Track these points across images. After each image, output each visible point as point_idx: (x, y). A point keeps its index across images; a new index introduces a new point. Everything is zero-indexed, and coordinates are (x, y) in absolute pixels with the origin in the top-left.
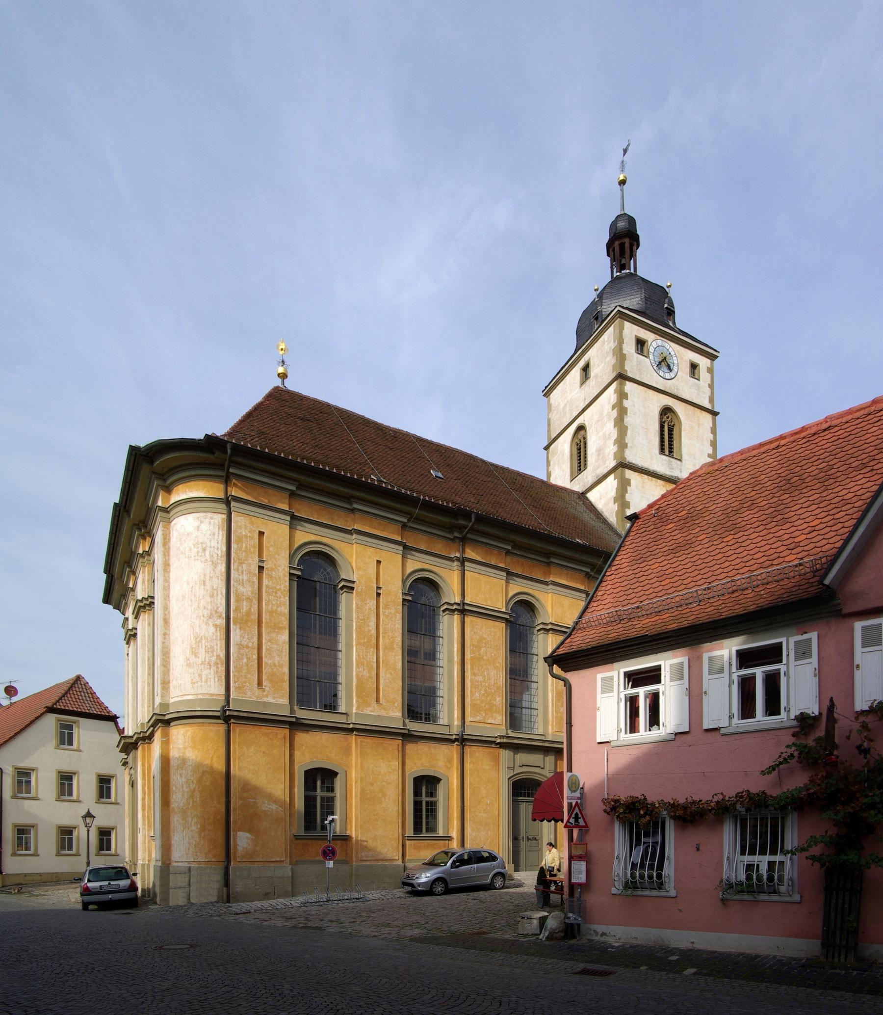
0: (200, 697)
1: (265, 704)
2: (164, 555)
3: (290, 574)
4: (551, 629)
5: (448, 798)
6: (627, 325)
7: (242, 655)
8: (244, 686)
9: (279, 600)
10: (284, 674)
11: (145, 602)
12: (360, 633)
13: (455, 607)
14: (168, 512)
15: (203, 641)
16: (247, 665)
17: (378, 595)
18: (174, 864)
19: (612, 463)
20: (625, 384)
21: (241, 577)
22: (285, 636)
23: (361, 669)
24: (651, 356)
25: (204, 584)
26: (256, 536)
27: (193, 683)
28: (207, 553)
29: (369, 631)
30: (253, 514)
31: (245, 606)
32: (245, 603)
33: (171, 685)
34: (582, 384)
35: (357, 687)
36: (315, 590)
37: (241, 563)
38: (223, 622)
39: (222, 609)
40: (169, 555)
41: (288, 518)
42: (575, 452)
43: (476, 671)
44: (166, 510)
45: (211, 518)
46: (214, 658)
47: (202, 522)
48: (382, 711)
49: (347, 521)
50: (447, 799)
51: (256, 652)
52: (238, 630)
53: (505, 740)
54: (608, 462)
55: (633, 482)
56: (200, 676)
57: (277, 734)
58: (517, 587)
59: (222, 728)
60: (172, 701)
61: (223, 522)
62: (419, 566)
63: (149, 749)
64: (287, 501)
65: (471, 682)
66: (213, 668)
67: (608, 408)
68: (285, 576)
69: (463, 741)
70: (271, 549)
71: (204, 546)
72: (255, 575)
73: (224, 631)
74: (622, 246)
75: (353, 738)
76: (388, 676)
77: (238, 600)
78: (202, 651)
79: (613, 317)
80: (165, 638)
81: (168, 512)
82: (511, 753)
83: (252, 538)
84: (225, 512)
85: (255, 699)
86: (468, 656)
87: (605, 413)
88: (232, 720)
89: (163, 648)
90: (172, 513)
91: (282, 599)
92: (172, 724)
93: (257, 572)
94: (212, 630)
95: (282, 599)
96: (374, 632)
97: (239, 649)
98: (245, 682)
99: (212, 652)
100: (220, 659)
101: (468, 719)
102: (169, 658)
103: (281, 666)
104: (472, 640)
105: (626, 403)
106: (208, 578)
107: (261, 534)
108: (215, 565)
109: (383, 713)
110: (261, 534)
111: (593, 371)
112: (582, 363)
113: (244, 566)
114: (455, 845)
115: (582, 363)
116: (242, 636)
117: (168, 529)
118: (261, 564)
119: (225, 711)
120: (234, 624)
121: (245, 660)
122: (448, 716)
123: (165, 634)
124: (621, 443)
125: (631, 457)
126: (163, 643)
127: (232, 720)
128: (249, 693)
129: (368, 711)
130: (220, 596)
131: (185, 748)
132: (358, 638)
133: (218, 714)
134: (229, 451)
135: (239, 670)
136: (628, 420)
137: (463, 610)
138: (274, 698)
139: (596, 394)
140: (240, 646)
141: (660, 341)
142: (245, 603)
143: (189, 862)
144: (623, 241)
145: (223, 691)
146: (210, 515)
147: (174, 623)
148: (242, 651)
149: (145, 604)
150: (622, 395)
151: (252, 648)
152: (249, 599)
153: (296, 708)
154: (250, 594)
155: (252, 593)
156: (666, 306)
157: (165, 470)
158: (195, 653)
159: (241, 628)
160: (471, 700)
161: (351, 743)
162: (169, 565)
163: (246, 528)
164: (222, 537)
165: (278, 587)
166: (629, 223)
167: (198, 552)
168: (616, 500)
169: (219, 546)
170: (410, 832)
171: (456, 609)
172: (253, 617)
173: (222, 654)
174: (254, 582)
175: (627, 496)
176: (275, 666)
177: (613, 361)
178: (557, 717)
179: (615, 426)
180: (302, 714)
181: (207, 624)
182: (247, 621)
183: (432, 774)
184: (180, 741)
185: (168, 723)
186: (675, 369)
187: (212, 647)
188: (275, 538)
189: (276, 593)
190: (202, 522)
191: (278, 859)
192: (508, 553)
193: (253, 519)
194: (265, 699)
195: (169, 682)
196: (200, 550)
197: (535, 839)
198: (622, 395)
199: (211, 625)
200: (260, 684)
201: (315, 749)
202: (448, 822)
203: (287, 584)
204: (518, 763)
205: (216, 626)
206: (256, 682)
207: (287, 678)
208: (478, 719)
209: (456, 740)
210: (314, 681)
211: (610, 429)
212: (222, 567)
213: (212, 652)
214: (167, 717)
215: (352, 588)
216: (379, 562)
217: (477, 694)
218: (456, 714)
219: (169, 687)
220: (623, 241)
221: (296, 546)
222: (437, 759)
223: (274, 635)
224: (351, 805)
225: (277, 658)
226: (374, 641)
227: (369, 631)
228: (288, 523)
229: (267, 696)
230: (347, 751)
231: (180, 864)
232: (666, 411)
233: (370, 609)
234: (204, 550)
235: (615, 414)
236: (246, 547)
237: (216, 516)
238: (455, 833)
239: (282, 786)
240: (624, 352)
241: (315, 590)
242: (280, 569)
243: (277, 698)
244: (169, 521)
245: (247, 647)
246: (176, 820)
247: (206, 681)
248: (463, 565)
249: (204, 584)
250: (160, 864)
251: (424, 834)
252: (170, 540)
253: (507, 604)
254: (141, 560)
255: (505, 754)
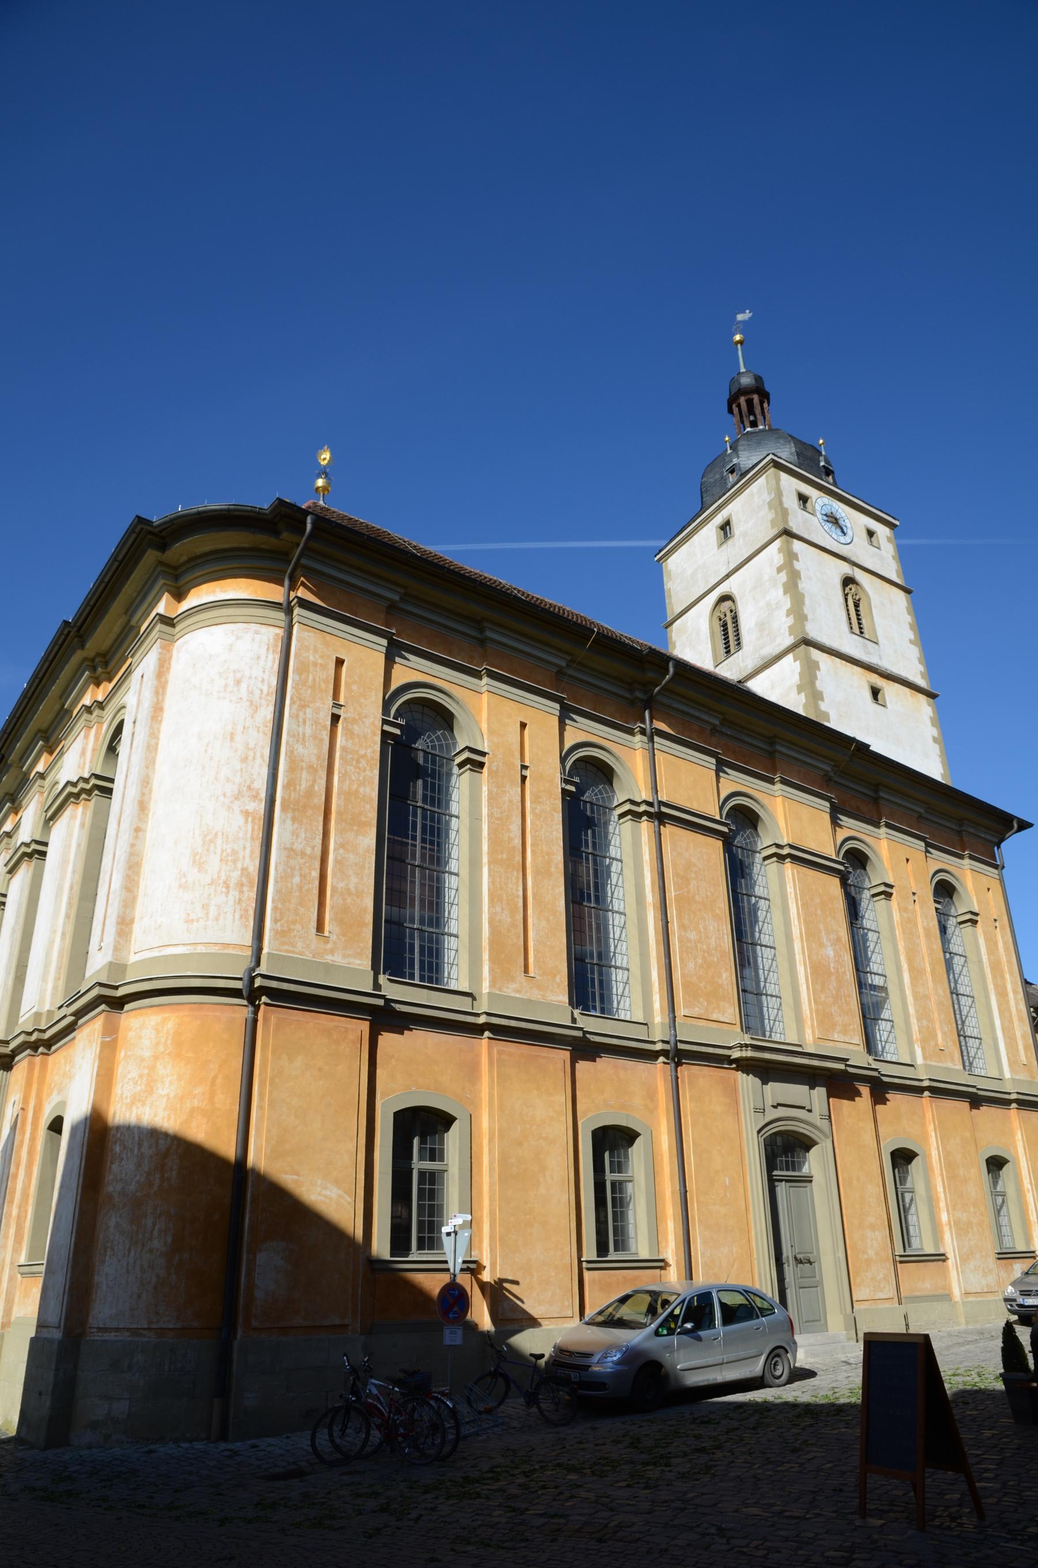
0: (201, 949)
1: (328, 968)
2: (157, 693)
3: (384, 732)
4: (789, 855)
5: (653, 1174)
6: (784, 476)
7: (293, 869)
8: (290, 930)
9: (361, 780)
10: (365, 910)
11: (81, 785)
12: (494, 842)
13: (643, 808)
14: (173, 626)
15: (219, 841)
16: (300, 889)
17: (524, 778)
18: (98, 1337)
19: (789, 641)
20: (792, 543)
21: (301, 730)
22: (369, 840)
23: (498, 909)
24: (818, 514)
25: (232, 739)
26: (332, 665)
27: (189, 921)
28: (244, 686)
29: (510, 839)
30: (329, 630)
31: (304, 780)
32: (304, 775)
33: (136, 927)
34: (720, 545)
35: (492, 942)
36: (415, 763)
37: (303, 707)
38: (261, 807)
39: (261, 785)
40: (164, 693)
41: (385, 642)
42: (719, 630)
43: (686, 922)
44: (168, 621)
45: (257, 632)
46: (236, 874)
47: (238, 638)
48: (535, 992)
49: (472, 657)
50: (647, 1171)
51: (317, 864)
52: (289, 822)
53: (749, 1053)
54: (778, 641)
55: (822, 665)
56: (205, 907)
57: (347, 1030)
58: (734, 782)
59: (247, 1012)
60: (133, 959)
61: (276, 640)
62: (582, 737)
63: (44, 1066)
64: (382, 616)
65: (680, 941)
66: (234, 894)
67: (769, 571)
68: (374, 734)
69: (679, 1056)
70: (355, 687)
71: (239, 675)
72: (324, 727)
73: (260, 824)
74: (750, 403)
75: (484, 1043)
76: (544, 923)
77: (292, 769)
78: (214, 862)
79: (764, 467)
80: (136, 838)
81: (173, 626)
82: (758, 1081)
83: (324, 667)
84: (282, 624)
85: (309, 956)
86: (671, 893)
87: (766, 577)
88: (264, 999)
89: (131, 854)
90: (178, 628)
91: (368, 773)
92: (127, 1007)
93: (329, 723)
94: (240, 820)
95: (368, 773)
96: (518, 842)
97: (288, 857)
98: (294, 922)
99: (235, 861)
100: (248, 875)
101: (681, 1011)
102: (138, 874)
103: (359, 894)
104: (674, 866)
105: (797, 565)
106: (240, 728)
107: (340, 662)
108: (255, 708)
109: (535, 995)
110: (340, 662)
111: (737, 528)
112: (719, 519)
113: (308, 711)
114: (673, 1278)
115: (719, 519)
116: (295, 834)
117: (169, 651)
118: (336, 711)
119: (252, 980)
120: (284, 808)
121: (297, 880)
122: (638, 1002)
123: (138, 830)
124: (798, 612)
125: (814, 632)
126: (133, 845)
127: (264, 999)
128: (300, 945)
129: (510, 990)
130: (258, 761)
131: (156, 1058)
132: (492, 851)
133: (238, 985)
134: (309, 527)
135: (283, 897)
136: (803, 585)
137: (661, 815)
138: (344, 956)
139: (746, 556)
140: (290, 852)
141: (826, 499)
142: (304, 775)
143: (134, 1332)
144: (750, 397)
145: (247, 938)
146: (254, 627)
147: (157, 808)
148: (292, 862)
149: (83, 790)
150: (791, 557)
151: (312, 857)
152: (311, 768)
153: (382, 979)
154: (314, 760)
155: (318, 758)
156: (822, 464)
157: (184, 558)
158: (199, 863)
159: (294, 819)
160: (683, 976)
161: (479, 1055)
162: (161, 709)
163: (316, 650)
164: (272, 662)
165: (362, 752)
166: (756, 379)
167: (226, 686)
168: (800, 689)
169: (266, 677)
170: (590, 1252)
171: (646, 813)
172: (316, 801)
173: (253, 866)
174: (322, 740)
175: (818, 684)
176: (350, 894)
177: (771, 515)
178: (817, 1011)
179: (785, 593)
180: (393, 990)
181: (230, 809)
182: (305, 807)
183: (624, 1124)
184: (146, 1042)
185: (118, 1004)
186: (849, 532)
187: (234, 852)
188: (358, 670)
189: (358, 762)
190: (238, 638)
191: (337, 1321)
192: (714, 730)
193: (328, 637)
194: (329, 958)
195: (132, 921)
196: (231, 682)
197: (811, 1263)
198: (791, 557)
199: (237, 809)
200: (320, 927)
201: (417, 1068)
202: (652, 1228)
203: (377, 748)
204: (769, 1102)
205: (246, 814)
206: (314, 924)
207: (369, 918)
208: (696, 1011)
209: (664, 1053)
210: (407, 931)
211: (778, 596)
212: (267, 713)
213: (235, 861)
214: (120, 992)
215: (481, 765)
216: (523, 726)
217: (691, 965)
218: (658, 1002)
219: (131, 932)
220: (750, 397)
221: (394, 687)
222: (617, 1091)
223: (350, 836)
224: (481, 1189)
225: (354, 880)
226: (519, 858)
227: (510, 839)
228: (384, 650)
229: (332, 952)
230: (472, 1071)
231: (111, 1336)
232: (848, 581)
233: (511, 801)
234: (238, 682)
235: (783, 577)
236: (314, 680)
237: (264, 629)
238: (671, 1252)
239: (352, 1146)
240: (786, 506)
241: (415, 763)
242: (368, 722)
243: (347, 959)
244: (172, 640)
245: (303, 854)
246: (113, 1224)
247: (217, 919)
248: (651, 740)
249: (232, 739)
250: (57, 1335)
251: (612, 1256)
252: (169, 669)
253: (721, 808)
254: (85, 716)
255: (747, 1082)
